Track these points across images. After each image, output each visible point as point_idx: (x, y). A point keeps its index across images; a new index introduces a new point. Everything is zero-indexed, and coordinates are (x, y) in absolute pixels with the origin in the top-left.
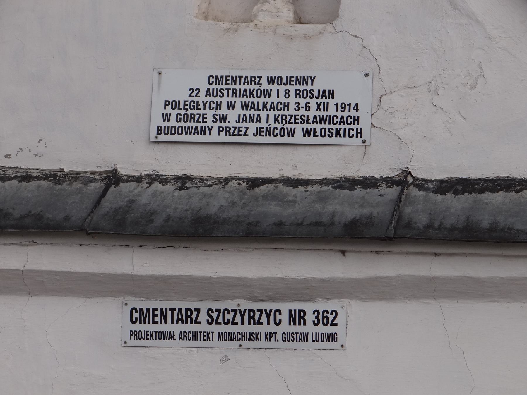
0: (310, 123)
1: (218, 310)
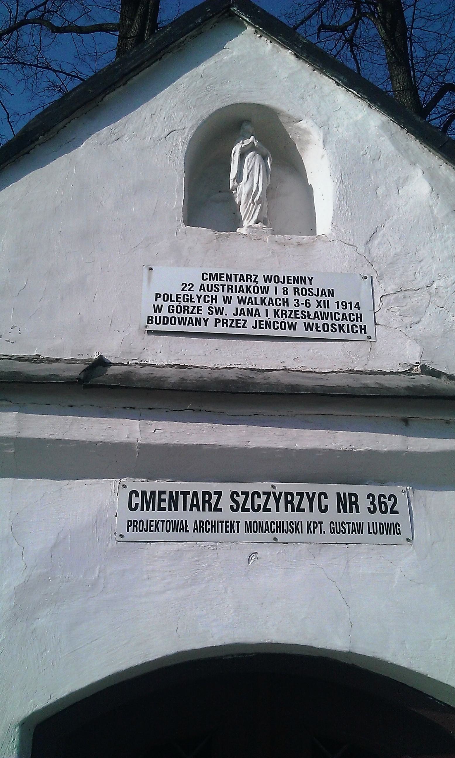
0: (312, 319)
1: (246, 494)
